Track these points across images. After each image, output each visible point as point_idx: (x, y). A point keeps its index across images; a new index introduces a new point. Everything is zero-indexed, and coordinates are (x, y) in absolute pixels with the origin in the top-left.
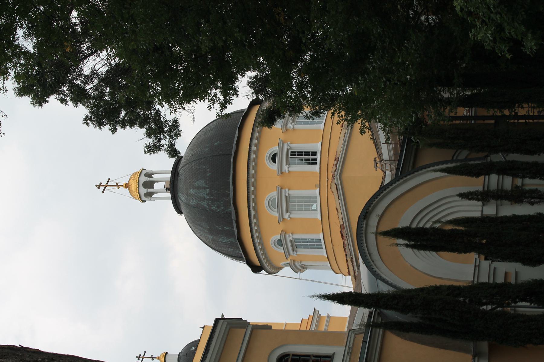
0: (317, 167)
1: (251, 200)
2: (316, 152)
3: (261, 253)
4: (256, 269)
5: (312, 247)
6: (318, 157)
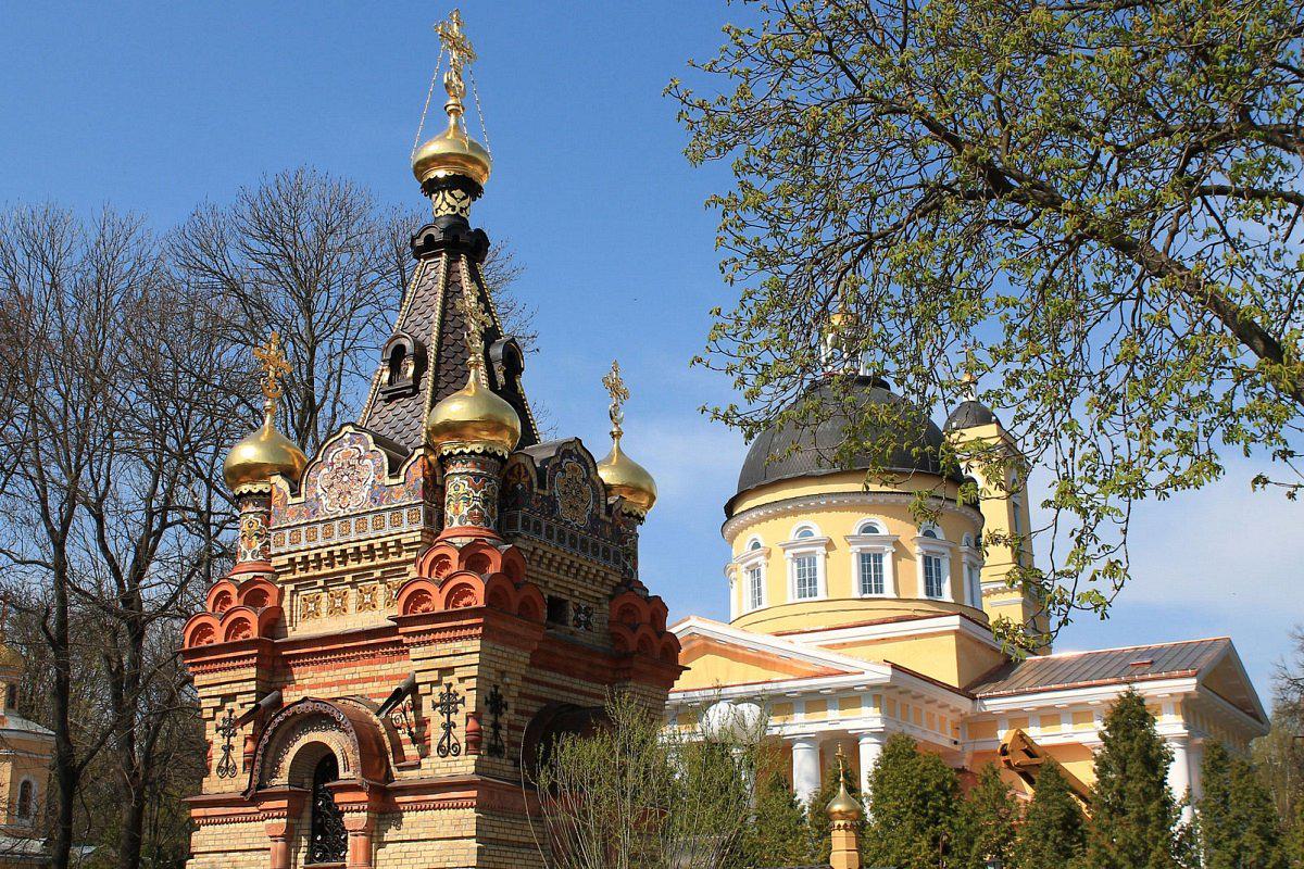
0: (791, 595)
1: (841, 499)
2: (816, 595)
3: (754, 515)
4: (729, 509)
5: (802, 583)
6: (808, 599)
